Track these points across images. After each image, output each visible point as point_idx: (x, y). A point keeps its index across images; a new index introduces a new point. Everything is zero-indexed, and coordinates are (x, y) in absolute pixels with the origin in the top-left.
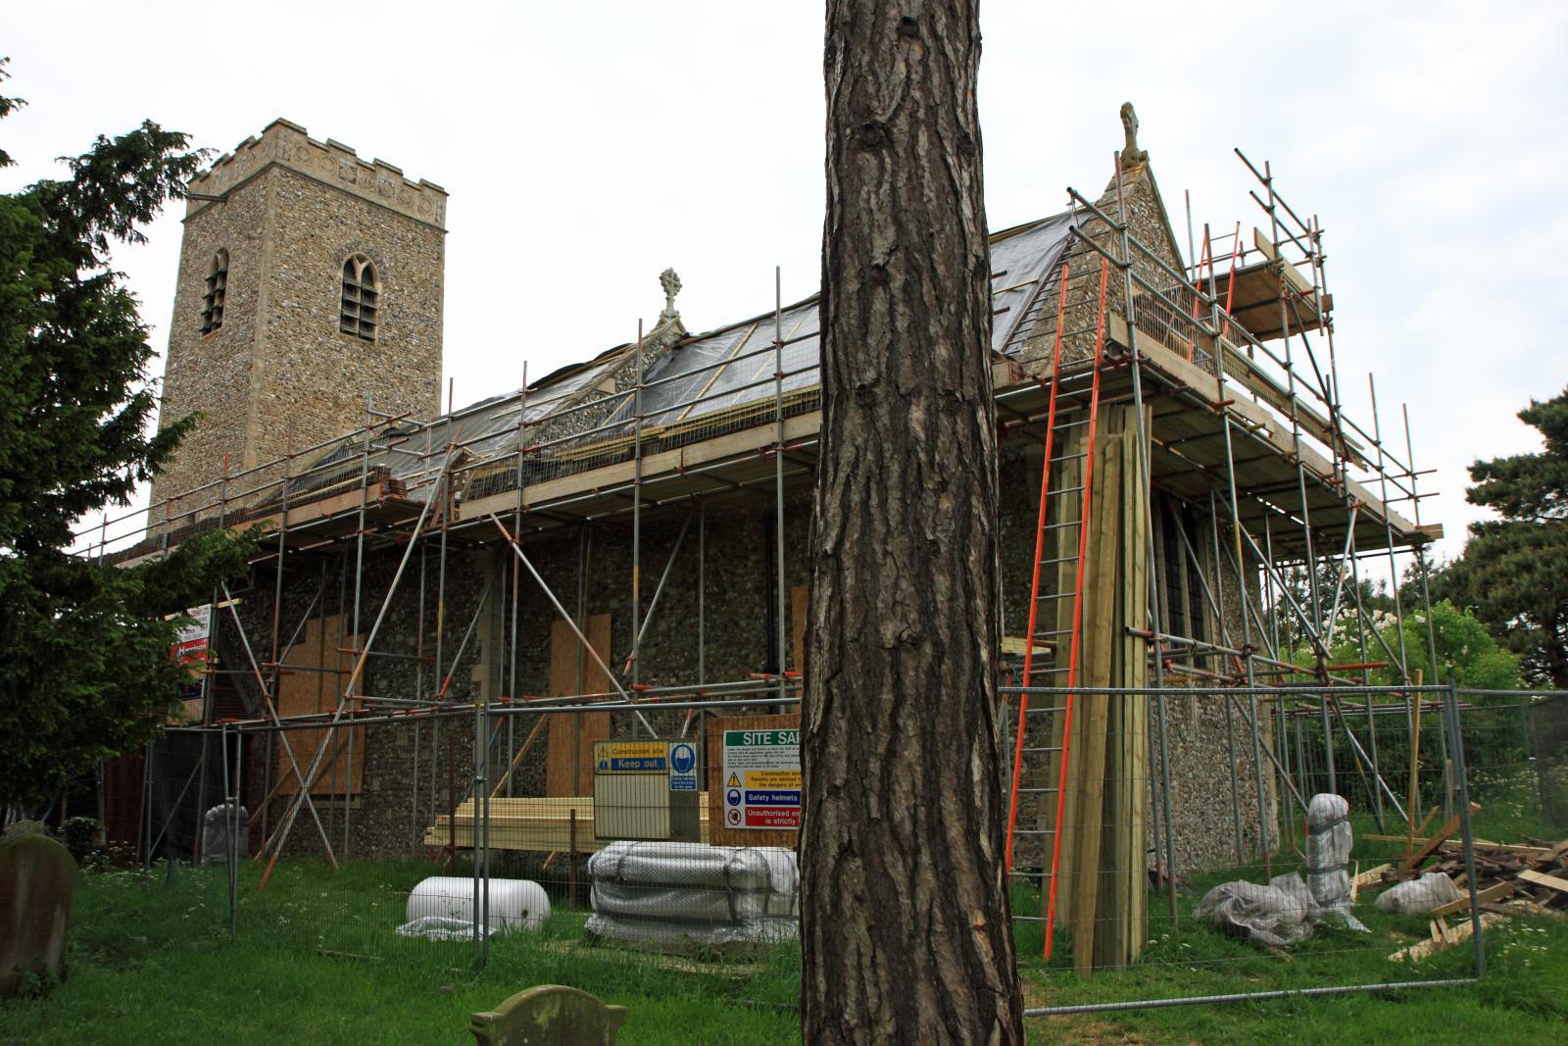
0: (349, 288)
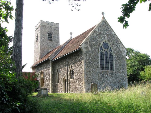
0: (49, 36)
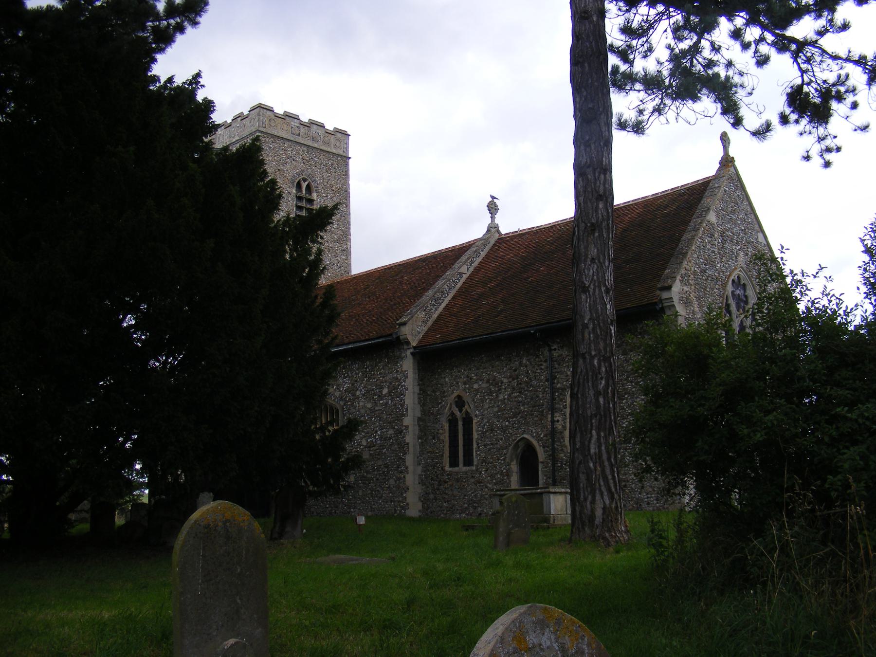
0: (299, 198)
